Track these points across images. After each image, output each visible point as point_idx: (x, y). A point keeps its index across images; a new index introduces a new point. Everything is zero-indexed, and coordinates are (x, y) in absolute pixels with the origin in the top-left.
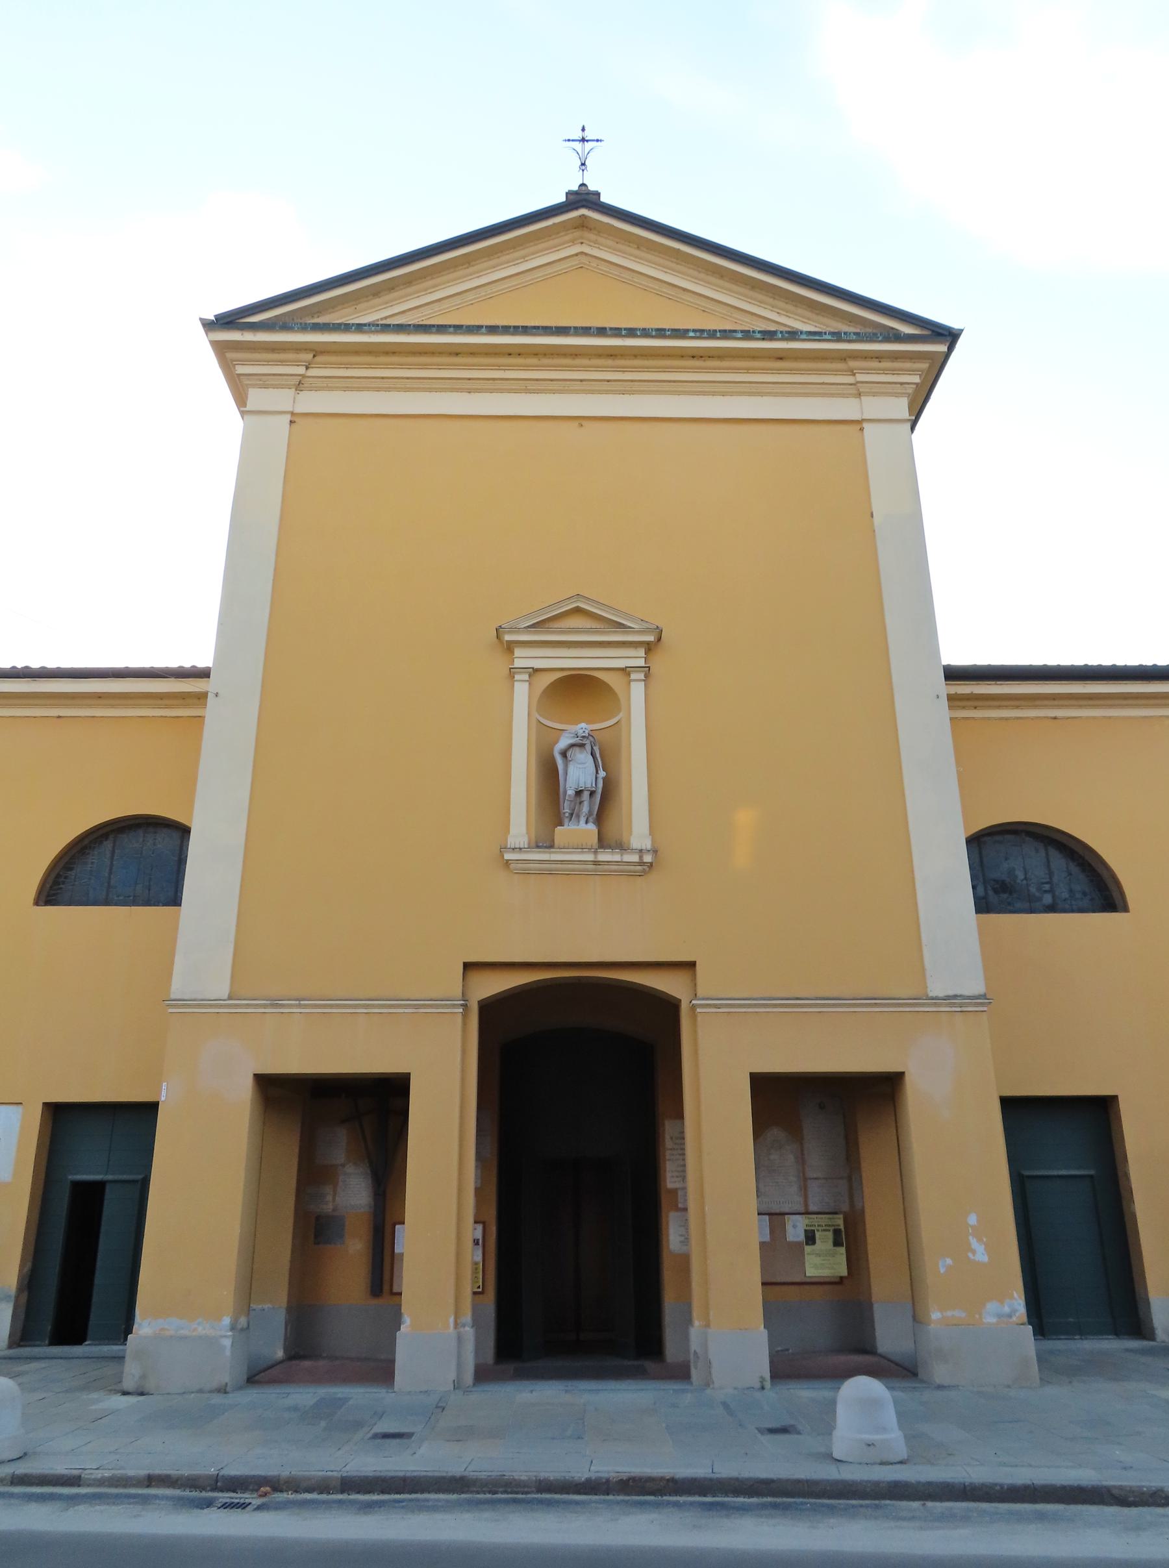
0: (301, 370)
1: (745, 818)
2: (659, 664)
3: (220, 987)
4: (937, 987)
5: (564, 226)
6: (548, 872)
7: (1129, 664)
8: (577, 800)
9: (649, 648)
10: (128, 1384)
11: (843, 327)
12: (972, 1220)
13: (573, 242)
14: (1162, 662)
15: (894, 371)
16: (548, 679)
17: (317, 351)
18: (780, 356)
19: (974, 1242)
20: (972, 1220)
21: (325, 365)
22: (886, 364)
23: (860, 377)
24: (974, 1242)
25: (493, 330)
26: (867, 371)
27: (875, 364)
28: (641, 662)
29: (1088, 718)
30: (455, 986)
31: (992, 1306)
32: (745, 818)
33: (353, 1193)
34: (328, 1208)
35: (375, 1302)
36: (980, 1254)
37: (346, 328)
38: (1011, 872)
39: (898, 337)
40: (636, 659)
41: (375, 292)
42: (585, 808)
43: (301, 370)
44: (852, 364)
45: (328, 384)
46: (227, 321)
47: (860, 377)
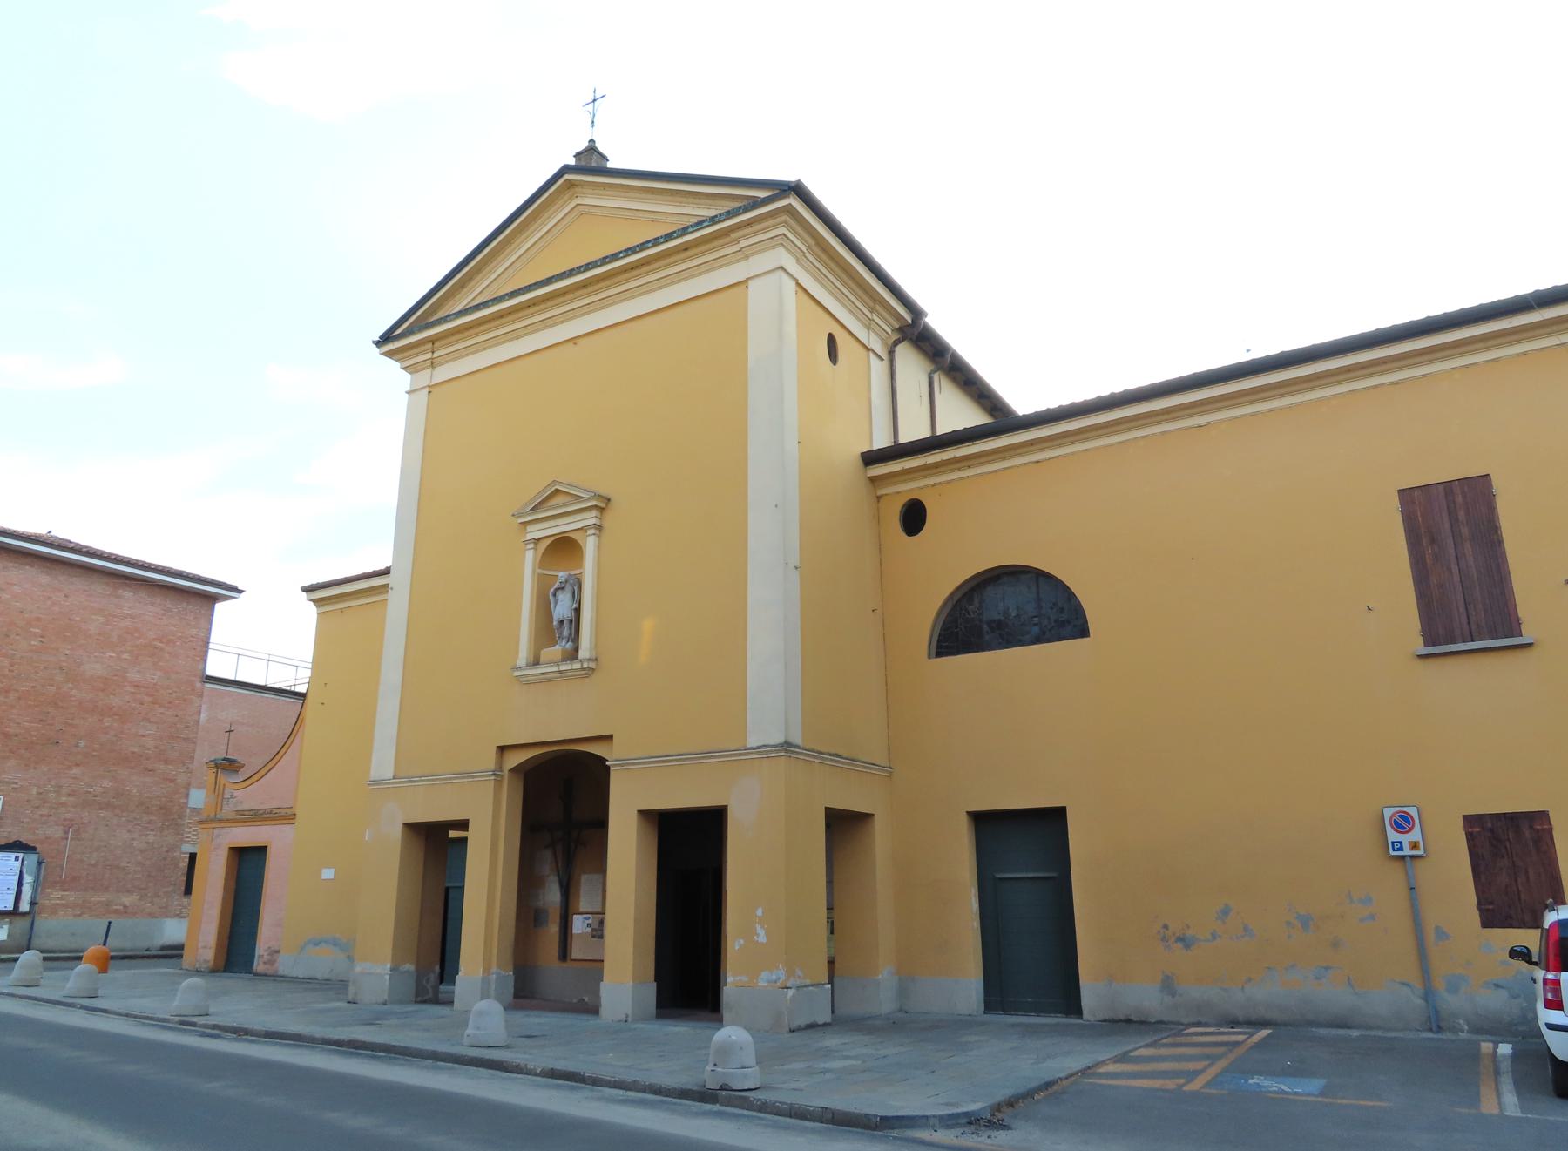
0: (429, 356)
1: (648, 625)
2: (609, 520)
3: (388, 772)
4: (753, 741)
5: (559, 192)
6: (540, 680)
7: (1382, 326)
8: (559, 631)
9: (601, 510)
10: (350, 998)
11: (762, 194)
12: (759, 912)
13: (571, 198)
14: (1560, 281)
15: (765, 230)
16: (544, 545)
17: (433, 340)
18: (685, 248)
19: (758, 927)
20: (759, 912)
21: (442, 347)
22: (756, 227)
23: (743, 244)
24: (758, 927)
25: (512, 294)
26: (745, 237)
27: (748, 230)
28: (593, 521)
29: (1097, 448)
30: (490, 761)
31: (765, 975)
32: (648, 625)
33: (552, 895)
34: (540, 904)
35: (564, 965)
36: (762, 937)
37: (445, 319)
38: (1006, 613)
39: (756, 203)
40: (590, 518)
41: (462, 285)
42: (566, 633)
43: (429, 356)
44: (733, 236)
45: (447, 359)
46: (386, 338)
47: (743, 244)
